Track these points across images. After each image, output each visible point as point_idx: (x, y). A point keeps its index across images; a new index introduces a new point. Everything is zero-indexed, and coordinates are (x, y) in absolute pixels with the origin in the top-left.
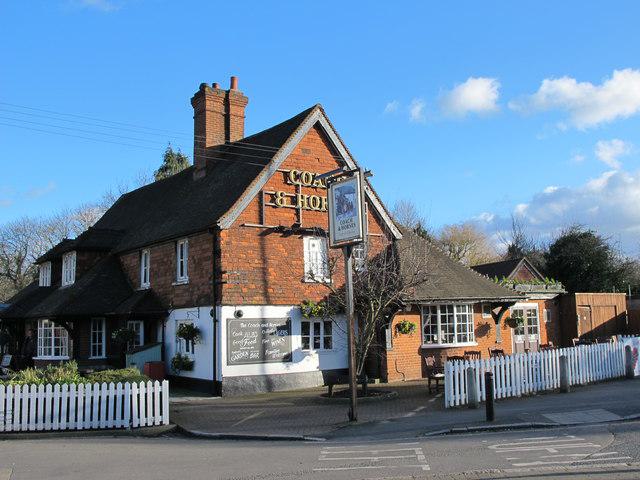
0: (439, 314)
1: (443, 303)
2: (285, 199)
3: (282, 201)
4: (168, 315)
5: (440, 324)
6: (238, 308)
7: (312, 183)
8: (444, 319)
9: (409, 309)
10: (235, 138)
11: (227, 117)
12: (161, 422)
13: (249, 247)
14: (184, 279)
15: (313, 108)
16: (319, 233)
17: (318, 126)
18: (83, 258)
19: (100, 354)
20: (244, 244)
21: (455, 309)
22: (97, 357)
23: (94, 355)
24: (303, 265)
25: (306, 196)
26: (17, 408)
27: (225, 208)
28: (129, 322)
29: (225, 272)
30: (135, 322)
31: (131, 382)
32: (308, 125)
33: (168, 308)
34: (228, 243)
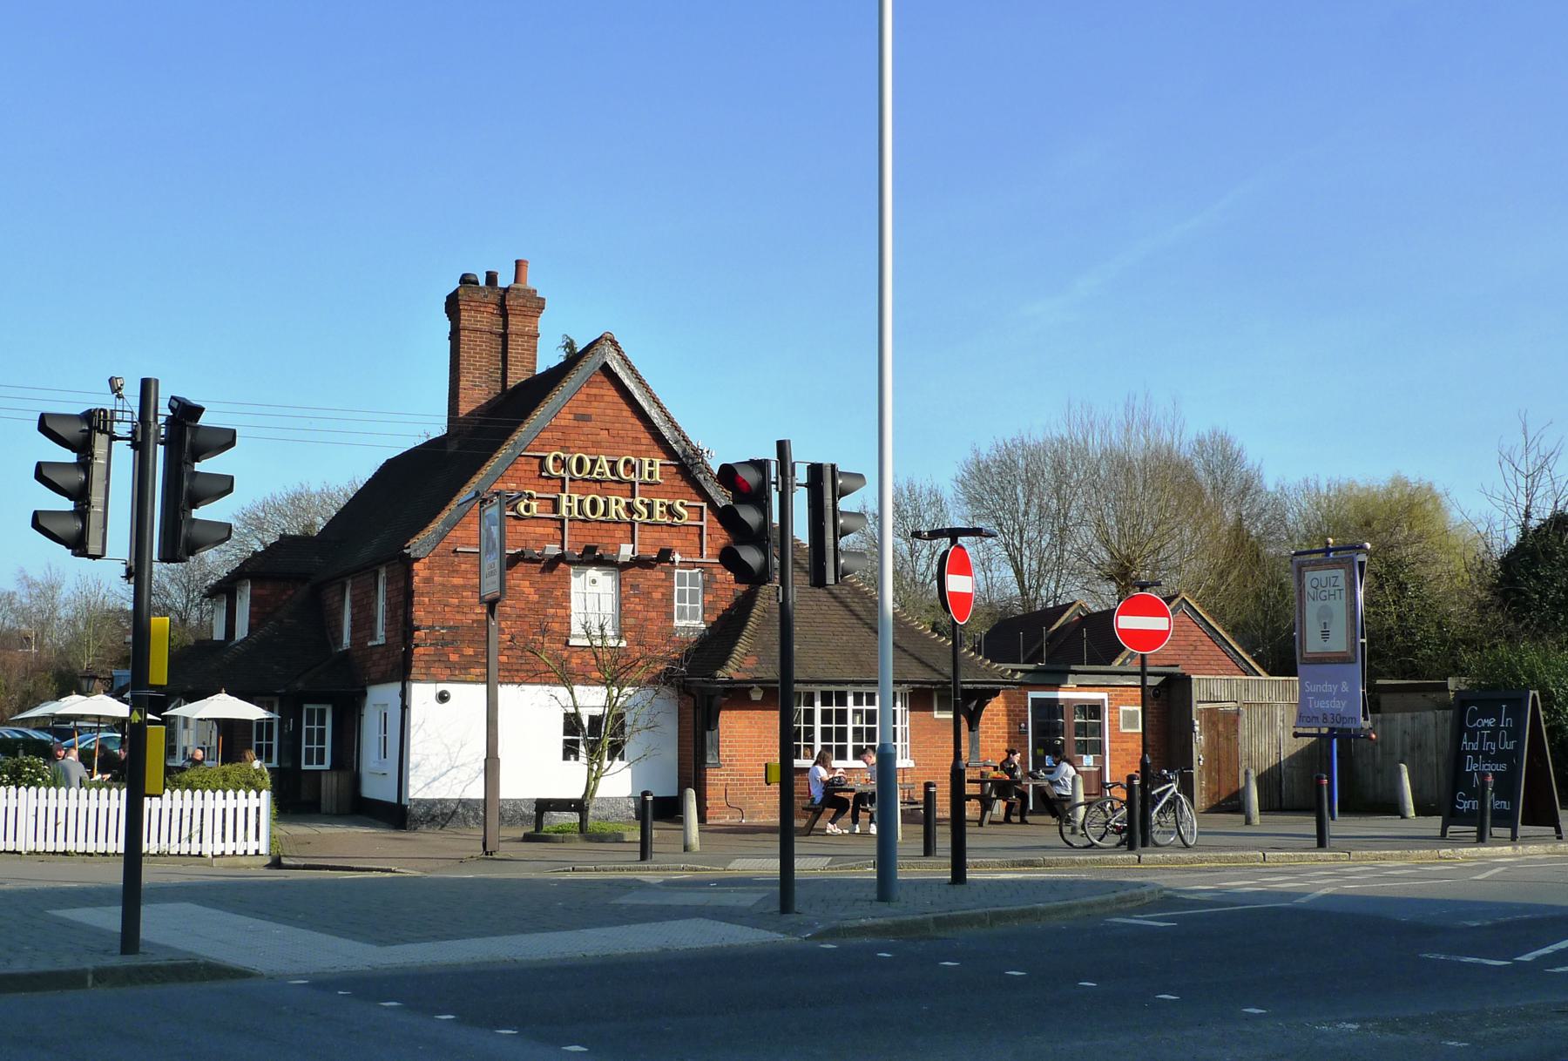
0: (818, 707)
1: (859, 689)
2: (534, 504)
3: (527, 508)
4: (365, 694)
5: (818, 725)
6: (442, 687)
7: (591, 473)
8: (826, 717)
9: (757, 696)
10: (511, 384)
11: (504, 337)
12: (257, 852)
13: (464, 587)
14: (381, 640)
15: (595, 342)
16: (591, 558)
17: (606, 370)
18: (259, 592)
19: (321, 761)
20: (457, 581)
21: (850, 699)
22: (315, 767)
23: (309, 762)
24: (569, 616)
25: (576, 497)
26: (61, 818)
27: (414, 534)
28: (306, 706)
29: (418, 629)
30: (316, 707)
31: (193, 790)
32: (589, 366)
33: (364, 687)
34: (428, 580)
